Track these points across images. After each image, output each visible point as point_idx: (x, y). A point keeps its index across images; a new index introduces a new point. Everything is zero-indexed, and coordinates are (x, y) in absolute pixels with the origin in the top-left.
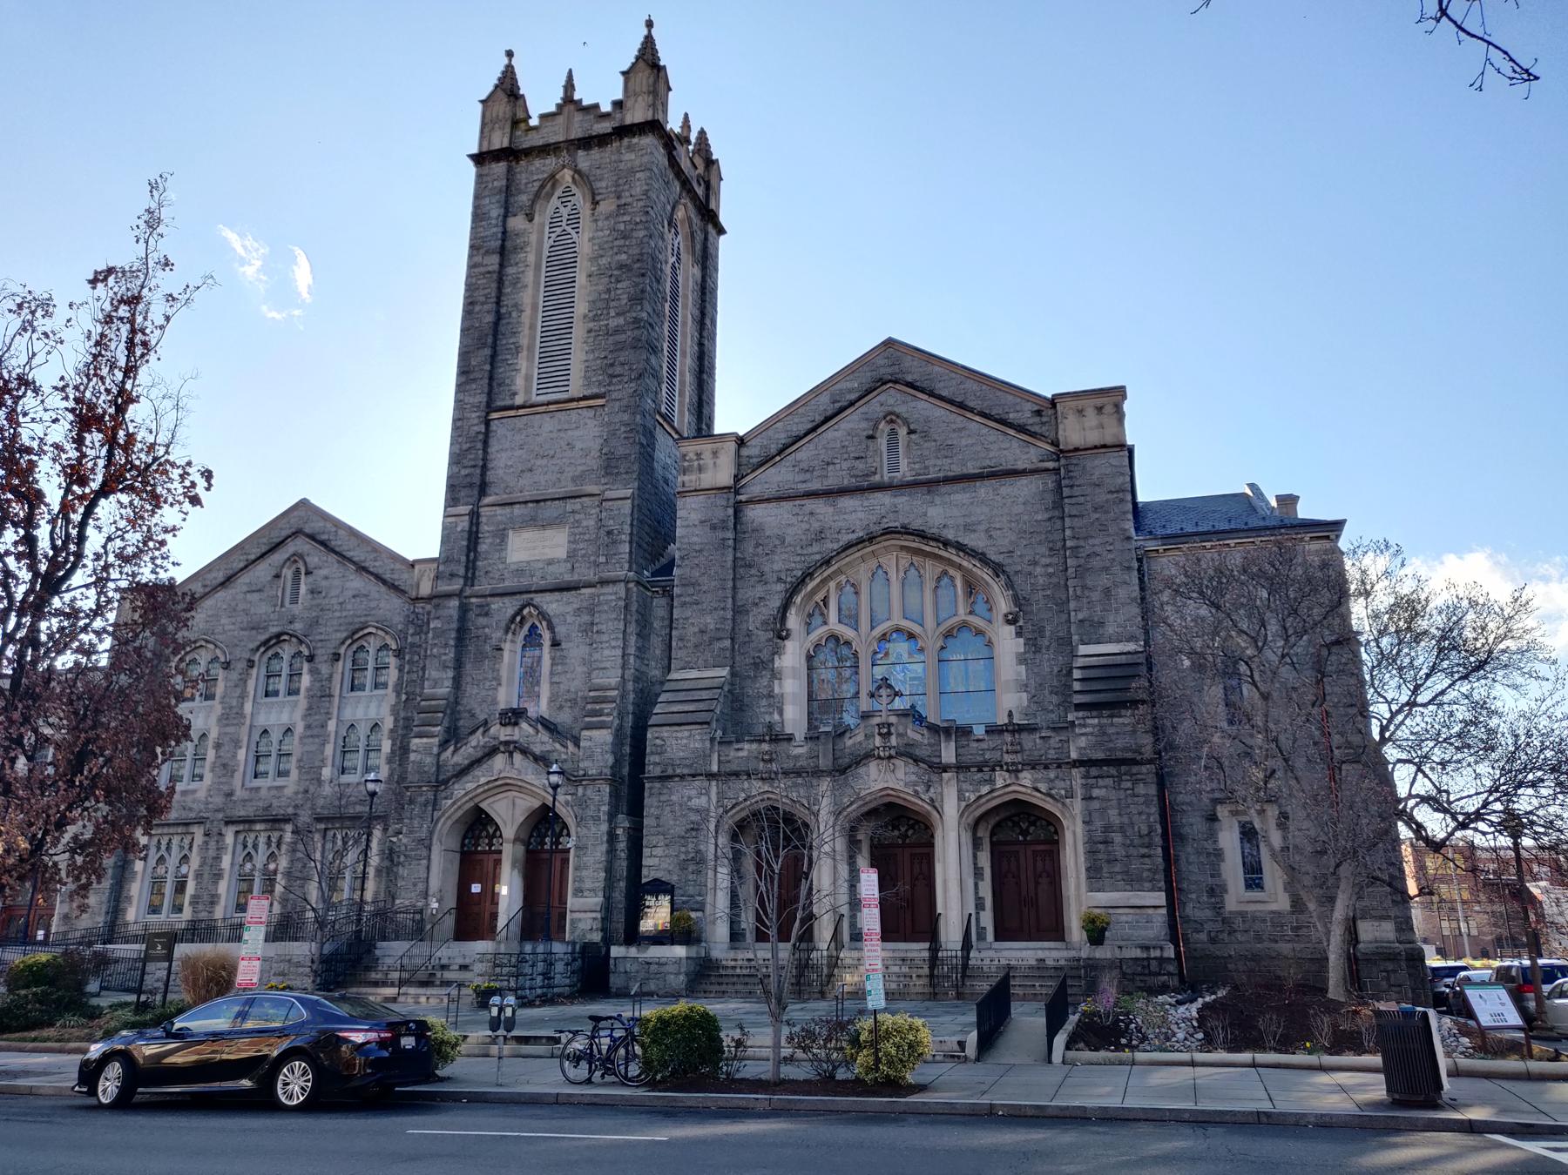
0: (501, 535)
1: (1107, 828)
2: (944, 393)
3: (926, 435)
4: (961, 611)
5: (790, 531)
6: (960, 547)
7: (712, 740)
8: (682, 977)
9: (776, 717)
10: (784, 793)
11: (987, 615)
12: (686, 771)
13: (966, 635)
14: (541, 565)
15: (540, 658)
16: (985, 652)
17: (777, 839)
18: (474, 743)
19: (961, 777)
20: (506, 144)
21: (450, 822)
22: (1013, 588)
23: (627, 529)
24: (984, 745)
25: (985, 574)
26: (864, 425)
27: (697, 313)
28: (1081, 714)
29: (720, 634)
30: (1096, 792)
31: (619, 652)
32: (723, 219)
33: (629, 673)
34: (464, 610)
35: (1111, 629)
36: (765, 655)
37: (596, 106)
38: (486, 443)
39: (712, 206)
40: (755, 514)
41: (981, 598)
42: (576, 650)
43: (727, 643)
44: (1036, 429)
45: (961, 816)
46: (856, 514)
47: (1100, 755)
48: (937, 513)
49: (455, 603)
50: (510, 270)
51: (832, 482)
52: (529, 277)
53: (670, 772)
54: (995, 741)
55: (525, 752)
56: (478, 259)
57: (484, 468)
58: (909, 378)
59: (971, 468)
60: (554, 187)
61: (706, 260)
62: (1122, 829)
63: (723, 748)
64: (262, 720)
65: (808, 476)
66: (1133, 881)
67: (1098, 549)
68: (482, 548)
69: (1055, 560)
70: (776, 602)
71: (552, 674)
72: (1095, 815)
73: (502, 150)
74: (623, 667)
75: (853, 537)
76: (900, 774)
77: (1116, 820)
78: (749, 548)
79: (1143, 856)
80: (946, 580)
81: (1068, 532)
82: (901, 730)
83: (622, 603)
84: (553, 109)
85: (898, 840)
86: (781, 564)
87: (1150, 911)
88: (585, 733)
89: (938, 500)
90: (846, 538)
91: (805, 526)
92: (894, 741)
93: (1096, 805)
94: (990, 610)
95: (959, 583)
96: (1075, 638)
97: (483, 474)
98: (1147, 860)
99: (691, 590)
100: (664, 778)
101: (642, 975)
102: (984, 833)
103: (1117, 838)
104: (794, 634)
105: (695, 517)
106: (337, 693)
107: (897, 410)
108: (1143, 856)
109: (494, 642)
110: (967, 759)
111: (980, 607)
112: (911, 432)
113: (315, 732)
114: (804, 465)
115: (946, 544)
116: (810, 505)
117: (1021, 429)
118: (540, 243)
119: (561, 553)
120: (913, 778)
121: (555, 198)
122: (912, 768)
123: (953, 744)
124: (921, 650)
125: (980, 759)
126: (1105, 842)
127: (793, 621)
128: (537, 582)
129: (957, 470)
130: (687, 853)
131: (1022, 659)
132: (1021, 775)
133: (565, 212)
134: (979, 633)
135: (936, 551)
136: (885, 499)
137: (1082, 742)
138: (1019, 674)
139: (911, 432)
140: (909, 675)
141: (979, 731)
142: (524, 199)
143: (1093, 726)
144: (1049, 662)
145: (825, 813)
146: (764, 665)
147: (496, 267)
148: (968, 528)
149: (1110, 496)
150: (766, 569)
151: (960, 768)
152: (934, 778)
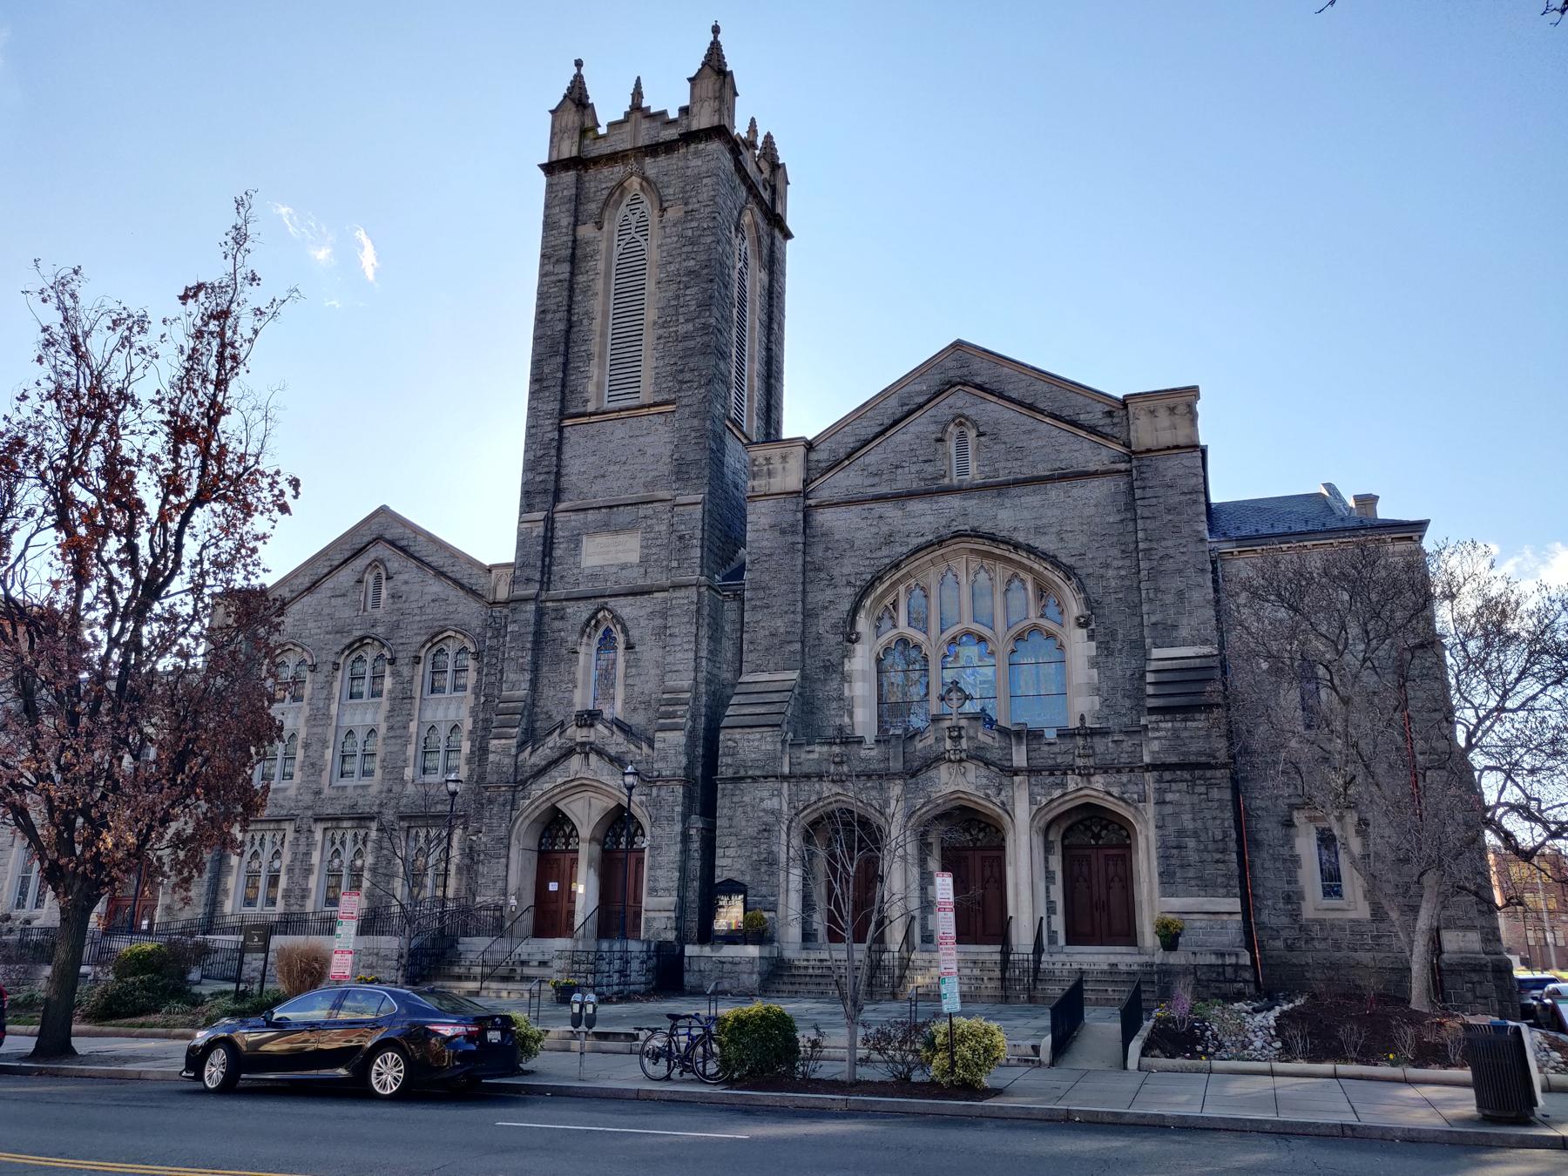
0: (575, 541)
1: (1181, 833)
2: (1014, 395)
3: (995, 438)
4: (1032, 614)
5: (859, 534)
6: (1030, 550)
7: (784, 742)
8: (755, 977)
9: (847, 720)
10: (854, 796)
11: (1058, 618)
12: (758, 773)
13: (1037, 639)
14: (614, 570)
15: (614, 661)
16: (1056, 655)
17: (848, 841)
18: (551, 744)
19: (1033, 780)
20: (574, 153)
21: (527, 822)
22: (1084, 590)
23: (699, 534)
24: (1056, 749)
25: (1056, 577)
26: (933, 428)
27: (764, 318)
28: (1154, 718)
29: (790, 638)
30: (1169, 797)
31: (691, 655)
32: (790, 223)
33: (702, 676)
34: (540, 613)
35: (1184, 632)
36: (834, 658)
37: (664, 113)
38: (559, 449)
39: (779, 210)
40: (824, 518)
41: (1052, 601)
42: (649, 652)
43: (798, 646)
44: (1108, 430)
45: (1033, 820)
46: (925, 517)
47: (1174, 759)
48: (1007, 516)
49: (531, 607)
50: (581, 278)
51: (901, 485)
52: (599, 286)
53: (742, 773)
54: (1068, 744)
55: (600, 753)
56: (549, 268)
57: (558, 475)
58: (978, 380)
59: (1042, 470)
60: (622, 194)
61: (773, 265)
62: (1196, 834)
63: (795, 750)
64: (347, 721)
65: (877, 480)
66: (1206, 886)
67: (1171, 552)
68: (557, 553)
69: (1127, 562)
70: (846, 606)
71: (626, 676)
72: (1168, 820)
73: (570, 159)
74: (696, 670)
75: (922, 540)
76: (971, 776)
77: (1189, 825)
78: (818, 552)
79: (1217, 861)
80: (1016, 583)
81: (1141, 535)
82: (972, 733)
83: (694, 607)
84: (621, 117)
85: (970, 844)
86: (851, 568)
87: (1225, 917)
88: (659, 735)
89: (1008, 502)
90: (916, 541)
91: (873, 530)
92: (964, 744)
93: (1168, 809)
94: (1062, 613)
95: (1030, 586)
96: (1148, 641)
97: (557, 480)
98: (1221, 866)
99: (761, 594)
100: (737, 779)
101: (714, 975)
102: (1056, 836)
103: (1191, 843)
104: (864, 638)
105: (765, 521)
106: (418, 695)
107: (966, 412)
108: (1217, 861)
109: (570, 645)
110: (1039, 763)
111: (1052, 611)
112: (980, 435)
113: (398, 732)
114: (872, 469)
115: (1017, 547)
116: (879, 508)
117: (1092, 430)
118: (610, 250)
119: (634, 558)
120: (984, 781)
121: (625, 203)
122: (983, 771)
123: (1024, 747)
124: (992, 654)
125: (1051, 762)
126: (1177, 847)
127: (863, 624)
128: (611, 586)
129: (1027, 472)
130: (759, 853)
131: (1094, 663)
132: (1093, 779)
133: (633, 219)
134: (1050, 636)
135: (1007, 554)
136: (954, 502)
137: (1155, 746)
138: (1091, 677)
139: (980, 435)
140: (980, 678)
141: (1051, 735)
142: (593, 207)
143: (1167, 730)
144: (1121, 666)
145: (896, 813)
146: (835, 668)
147: (567, 276)
148: (1040, 531)
149: (1182, 498)
150: (835, 573)
151: (1032, 771)
152: (1005, 781)
